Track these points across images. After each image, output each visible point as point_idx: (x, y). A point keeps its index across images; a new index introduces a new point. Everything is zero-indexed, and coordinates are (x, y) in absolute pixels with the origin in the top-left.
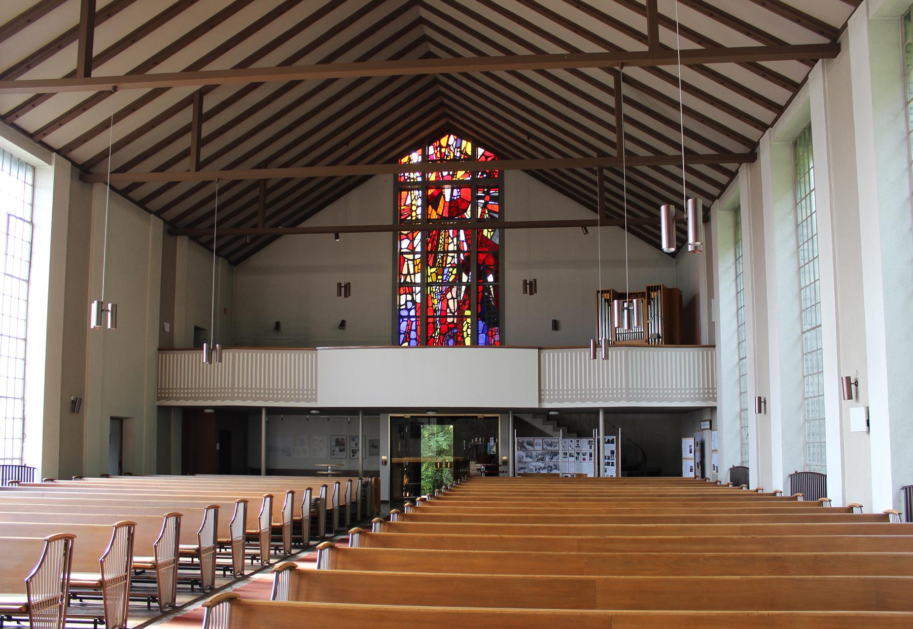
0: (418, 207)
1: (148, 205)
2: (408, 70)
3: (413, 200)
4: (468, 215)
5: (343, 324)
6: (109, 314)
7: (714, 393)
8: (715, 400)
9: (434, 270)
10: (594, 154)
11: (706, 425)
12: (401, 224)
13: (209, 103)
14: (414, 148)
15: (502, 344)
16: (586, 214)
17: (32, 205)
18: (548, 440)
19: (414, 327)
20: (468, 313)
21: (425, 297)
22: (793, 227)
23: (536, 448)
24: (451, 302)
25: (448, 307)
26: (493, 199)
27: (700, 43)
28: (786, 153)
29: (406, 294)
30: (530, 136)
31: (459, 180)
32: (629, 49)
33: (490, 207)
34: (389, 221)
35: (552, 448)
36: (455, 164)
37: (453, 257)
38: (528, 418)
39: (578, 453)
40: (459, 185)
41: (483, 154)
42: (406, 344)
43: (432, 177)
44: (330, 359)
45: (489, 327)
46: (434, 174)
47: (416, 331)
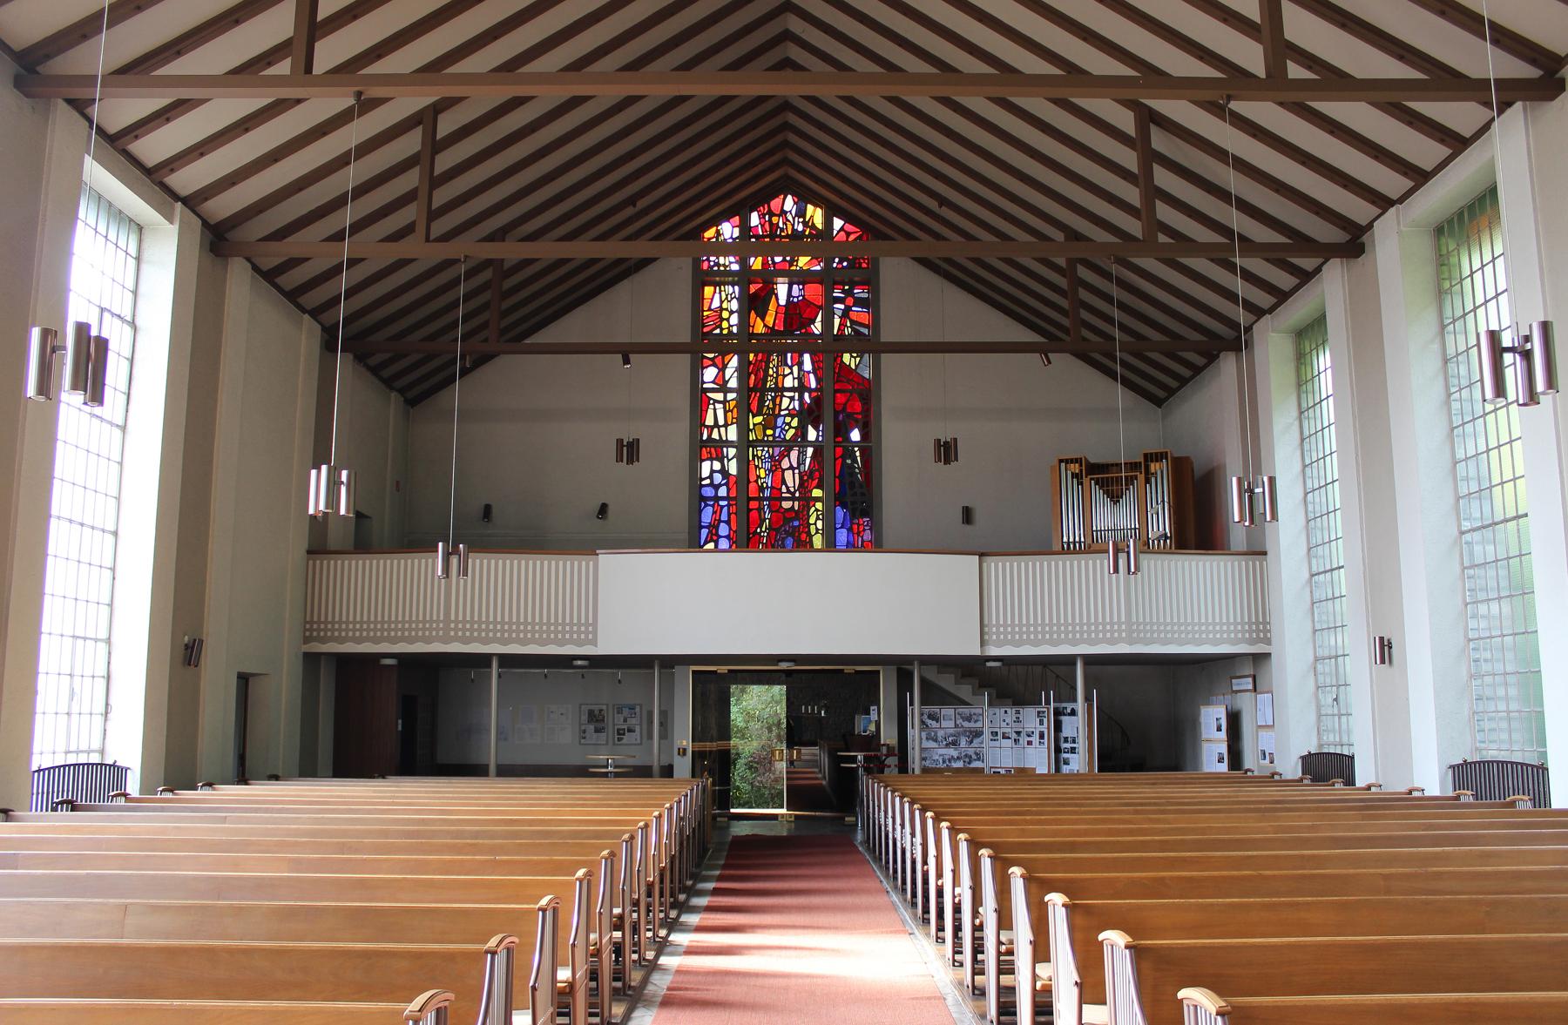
0: (732, 312)
1: (302, 300)
2: (746, 87)
3: (723, 301)
4: (817, 327)
5: (603, 510)
6: (343, 489)
7: (1267, 631)
8: (1268, 642)
9: (759, 419)
10: (1059, 236)
11: (1247, 684)
12: (704, 342)
13: (447, 125)
14: (726, 216)
15: (877, 545)
17: (135, 293)
19: (724, 517)
20: (817, 493)
21: (744, 463)
22: (1439, 363)
23: (944, 724)
24: (788, 475)
25: (784, 482)
26: (860, 302)
27: (1309, 68)
28: (1423, 246)
29: (711, 459)
30: (943, 201)
33: (853, 316)
34: (685, 336)
35: (972, 725)
37: (792, 399)
39: (1018, 733)
40: (802, 278)
41: (842, 229)
42: (711, 546)
43: (756, 263)
44: (499, 575)
45: (853, 516)
47: (728, 522)
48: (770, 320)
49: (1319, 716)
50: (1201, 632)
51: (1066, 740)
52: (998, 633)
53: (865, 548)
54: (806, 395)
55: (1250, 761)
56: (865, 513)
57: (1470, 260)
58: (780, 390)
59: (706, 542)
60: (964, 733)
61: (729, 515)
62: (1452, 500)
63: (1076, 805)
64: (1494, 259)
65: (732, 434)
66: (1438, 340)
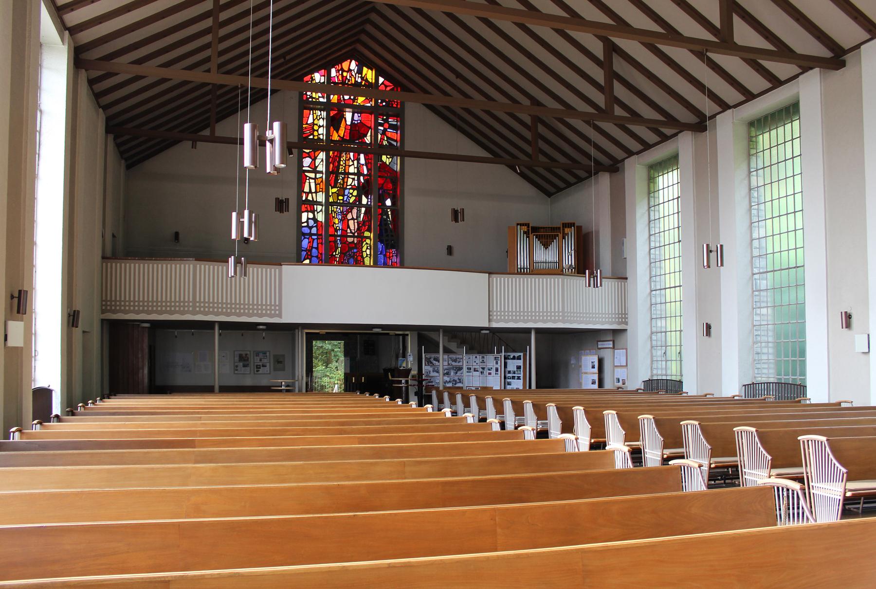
0: (320, 127)
3: (318, 120)
4: (368, 139)
8: (626, 323)
9: (335, 190)
10: (526, 102)
11: (610, 344)
14: (317, 70)
15: (402, 265)
16: (483, 154)
18: (454, 356)
19: (315, 245)
20: (367, 234)
22: (747, 190)
24: (351, 223)
25: (348, 227)
26: (392, 127)
27: (715, 35)
28: (743, 130)
29: (308, 212)
31: (360, 106)
32: (588, 17)
35: (457, 364)
36: (357, 88)
37: (353, 179)
38: (433, 335)
39: (483, 368)
41: (383, 83)
42: (307, 261)
45: (387, 248)
46: (336, 97)
47: (317, 248)
48: (341, 133)
49: (652, 361)
51: (509, 372)
52: (497, 315)
53: (393, 266)
54: (362, 178)
55: (608, 385)
56: (393, 247)
57: (764, 140)
58: (347, 174)
60: (453, 368)
64: (793, 139)
65: (321, 197)
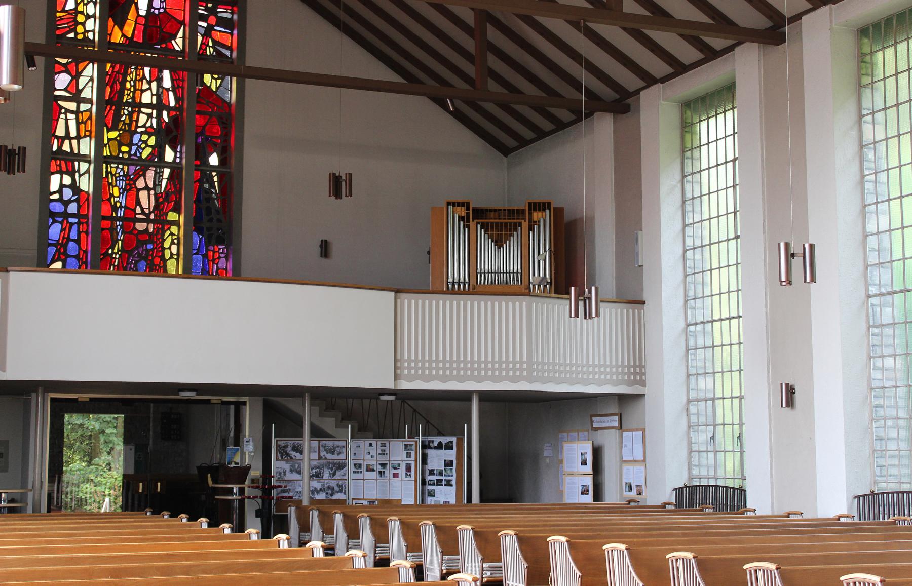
0: (88, 17)
4: (178, 44)
8: (643, 383)
9: (114, 134)
11: (614, 421)
15: (237, 275)
18: (329, 443)
19: (74, 235)
20: (172, 216)
21: (100, 181)
22: (856, 148)
24: (143, 195)
25: (138, 203)
26: (222, 22)
28: (848, 42)
29: (61, 173)
35: (335, 457)
37: (150, 116)
42: (58, 265)
45: (209, 242)
47: (77, 241)
48: (129, 29)
49: (690, 452)
50: (589, 373)
51: (431, 472)
52: (409, 368)
53: (220, 275)
54: (165, 114)
55: (611, 496)
56: (220, 241)
58: (138, 106)
59: (53, 262)
60: (327, 465)
61: (79, 233)
62: (861, 268)
63: (607, 530)
65: (87, 147)
66: (856, 126)
